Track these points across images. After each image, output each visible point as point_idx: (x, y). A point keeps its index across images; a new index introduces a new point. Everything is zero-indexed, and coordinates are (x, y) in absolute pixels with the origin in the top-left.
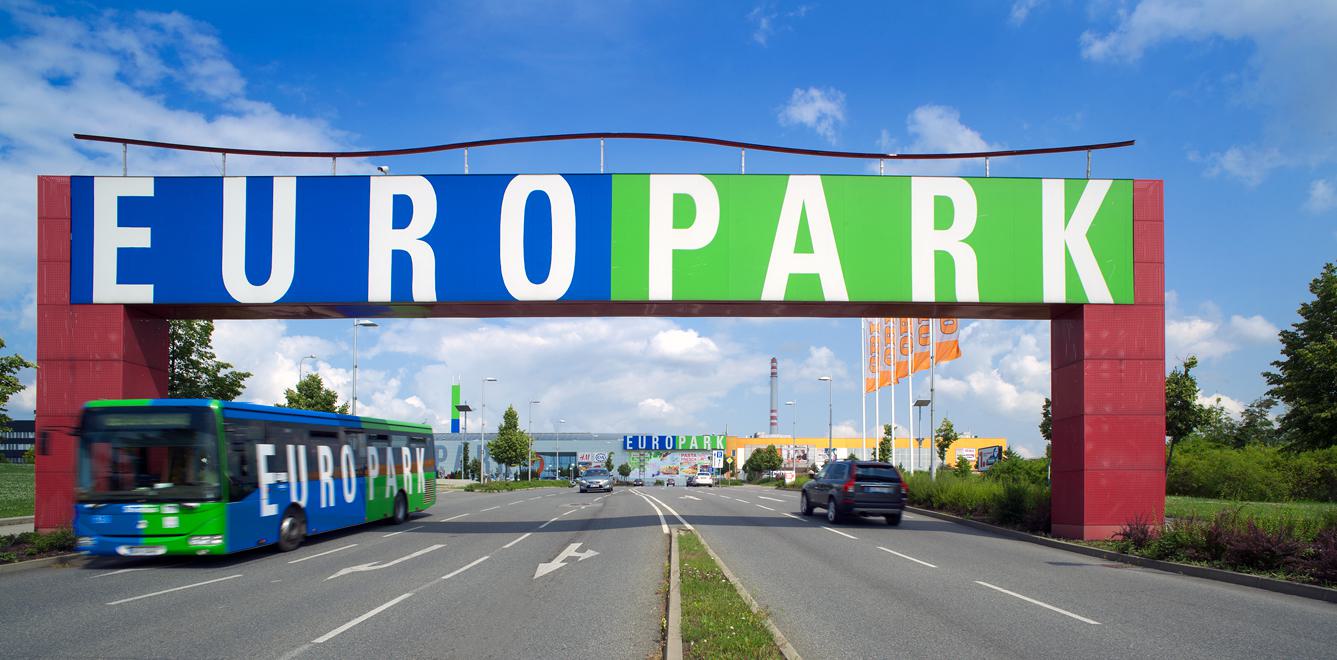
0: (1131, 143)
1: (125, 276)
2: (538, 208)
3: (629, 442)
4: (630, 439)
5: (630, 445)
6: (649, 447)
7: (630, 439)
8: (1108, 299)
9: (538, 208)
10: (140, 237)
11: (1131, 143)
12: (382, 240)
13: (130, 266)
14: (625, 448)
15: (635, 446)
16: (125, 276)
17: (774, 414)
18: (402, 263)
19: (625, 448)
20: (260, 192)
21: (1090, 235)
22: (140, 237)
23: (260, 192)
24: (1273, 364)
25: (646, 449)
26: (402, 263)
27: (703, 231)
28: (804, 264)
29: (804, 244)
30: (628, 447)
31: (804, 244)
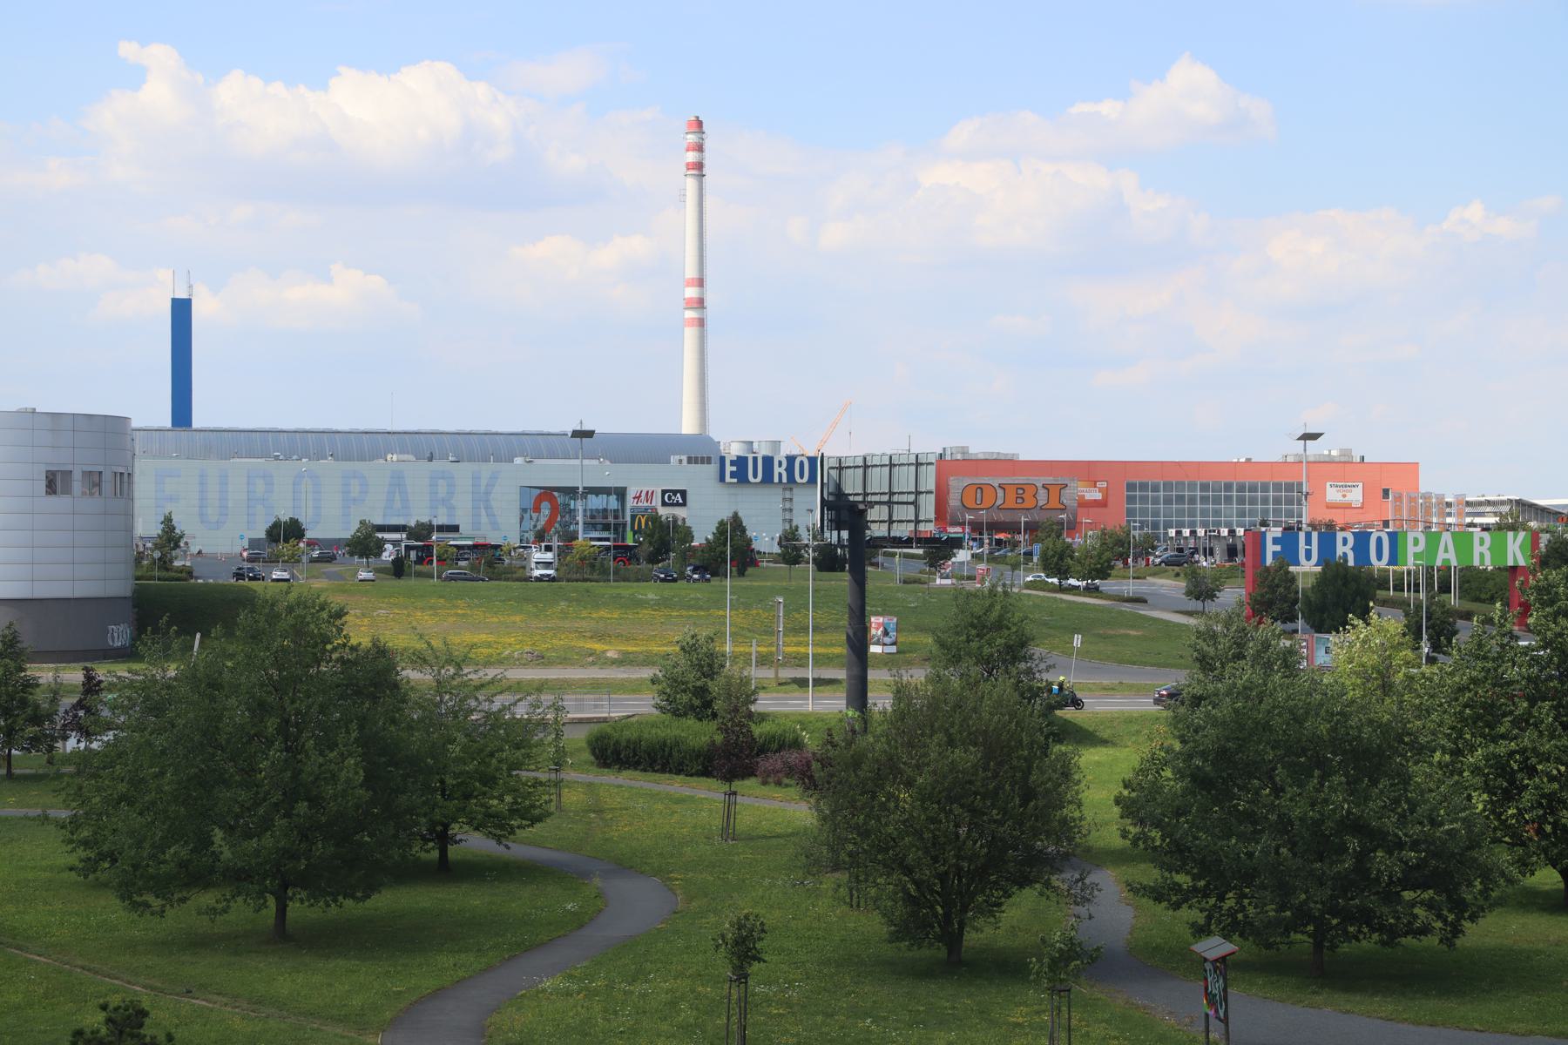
0: (181, 311)
1: (731, 477)
2: (755, 476)
3: (729, 469)
4: (732, 463)
5: (733, 475)
6: (768, 478)
7: (732, 463)
8: (1524, 564)
9: (755, 476)
10: (734, 469)
11: (181, 311)
12: (777, 470)
13: (733, 475)
14: (722, 479)
15: (741, 475)
16: (731, 477)
17: (788, 505)
18: (780, 475)
19: (722, 479)
20: (755, 459)
21: (1520, 547)
22: (734, 469)
23: (755, 459)
24: (432, 453)
25: (808, 482)
26: (780, 475)
27: (1421, 547)
28: (1446, 556)
29: (1446, 551)
30: (728, 479)
31: (1446, 551)
